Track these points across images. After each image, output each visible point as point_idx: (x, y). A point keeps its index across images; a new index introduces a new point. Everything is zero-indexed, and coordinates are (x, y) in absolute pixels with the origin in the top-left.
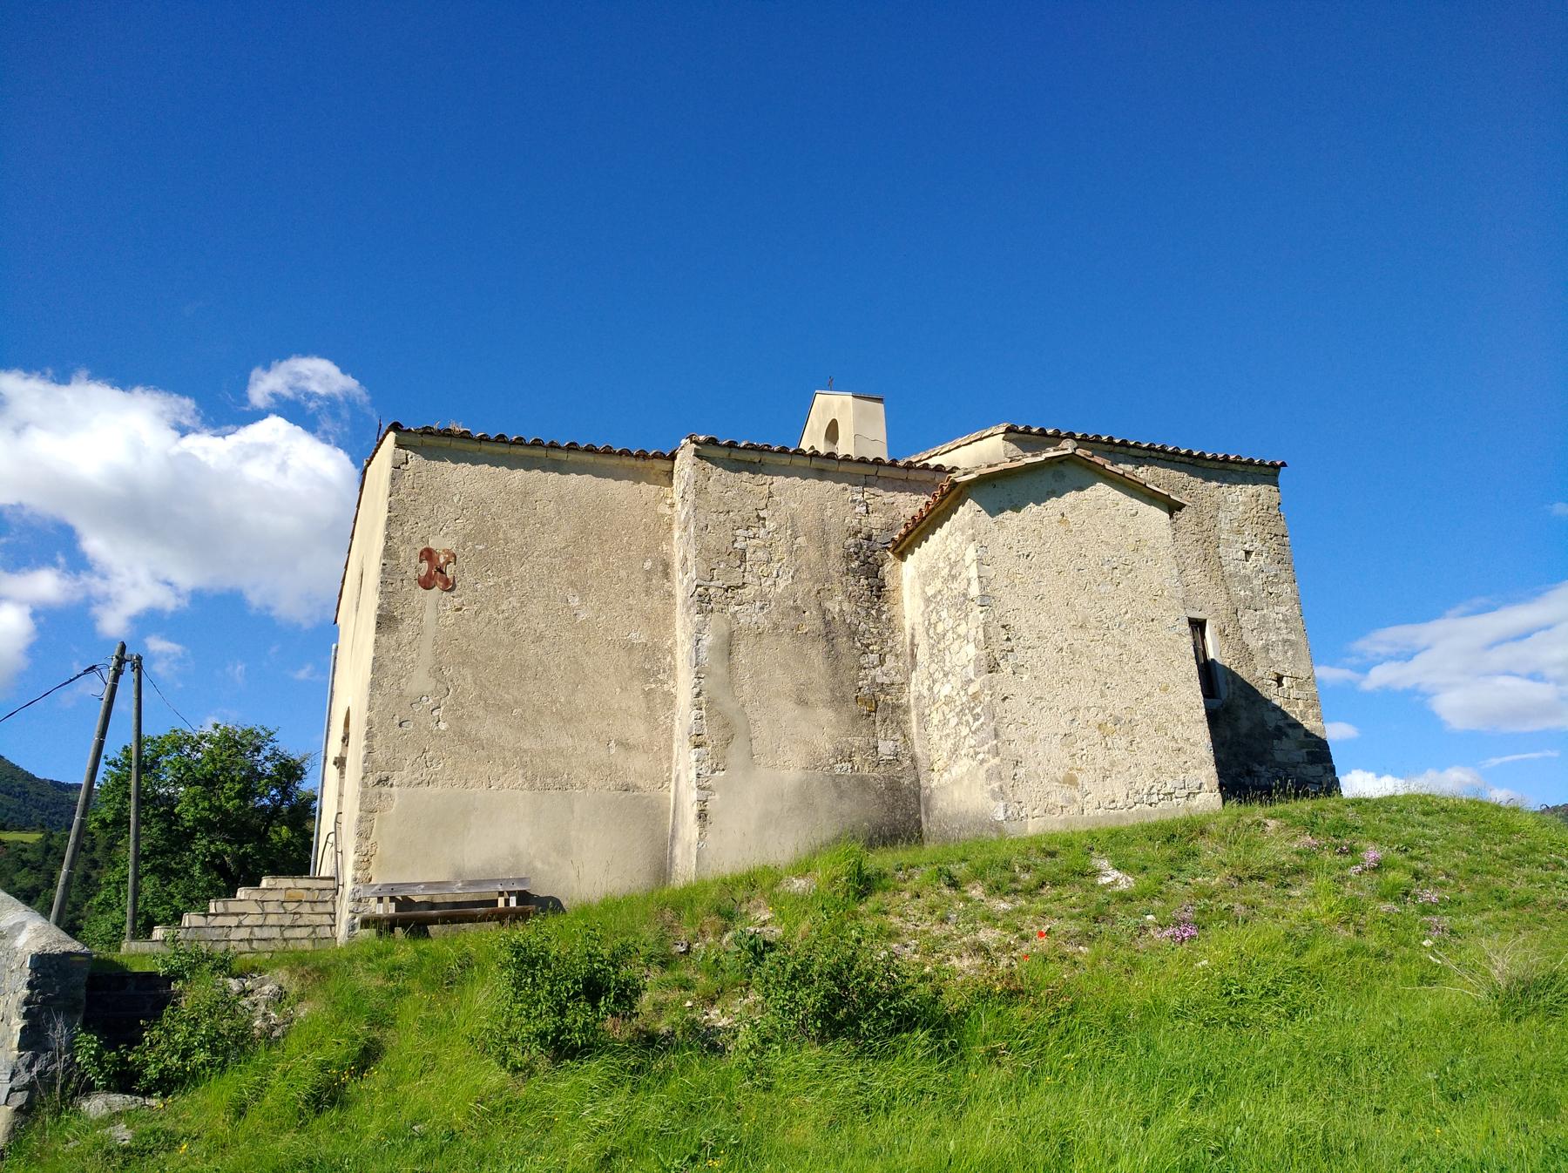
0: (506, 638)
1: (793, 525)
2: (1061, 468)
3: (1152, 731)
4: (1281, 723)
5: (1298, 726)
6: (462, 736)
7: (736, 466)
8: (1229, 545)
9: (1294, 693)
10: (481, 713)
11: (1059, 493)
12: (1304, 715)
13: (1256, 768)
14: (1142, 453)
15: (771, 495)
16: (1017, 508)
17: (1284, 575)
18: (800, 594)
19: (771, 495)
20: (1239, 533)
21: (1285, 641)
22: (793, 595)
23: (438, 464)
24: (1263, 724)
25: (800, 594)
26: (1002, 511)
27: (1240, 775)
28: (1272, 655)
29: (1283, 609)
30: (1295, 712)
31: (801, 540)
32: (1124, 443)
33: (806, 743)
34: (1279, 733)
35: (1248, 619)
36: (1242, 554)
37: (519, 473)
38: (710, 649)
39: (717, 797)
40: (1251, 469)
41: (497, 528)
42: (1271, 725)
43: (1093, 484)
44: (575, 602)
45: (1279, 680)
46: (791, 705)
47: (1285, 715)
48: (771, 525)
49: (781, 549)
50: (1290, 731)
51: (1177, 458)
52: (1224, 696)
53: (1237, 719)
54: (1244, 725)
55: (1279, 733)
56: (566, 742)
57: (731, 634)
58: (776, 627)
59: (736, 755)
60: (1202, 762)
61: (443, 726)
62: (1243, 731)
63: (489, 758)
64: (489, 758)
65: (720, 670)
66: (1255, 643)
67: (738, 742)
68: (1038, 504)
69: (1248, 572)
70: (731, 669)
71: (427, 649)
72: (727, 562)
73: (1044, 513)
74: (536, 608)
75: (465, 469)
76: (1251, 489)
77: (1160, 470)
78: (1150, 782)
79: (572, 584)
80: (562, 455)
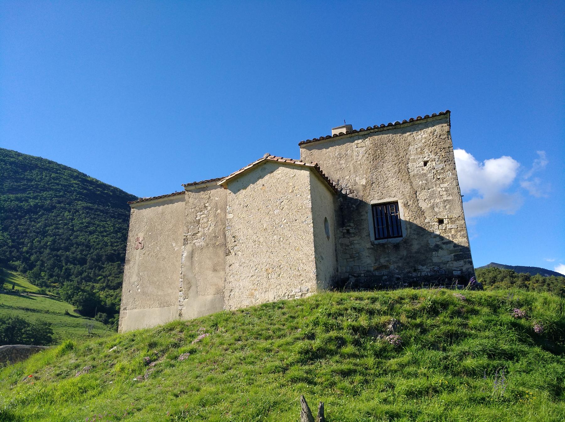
0: (155, 260)
1: (217, 206)
2: (265, 166)
3: (289, 269)
4: (439, 243)
5: (450, 242)
6: (144, 293)
7: (198, 191)
8: (414, 160)
9: (449, 226)
10: (148, 285)
11: (261, 177)
12: (454, 236)
13: (420, 267)
14: (366, 133)
15: (210, 197)
16: (245, 188)
17: (448, 167)
18: (217, 231)
19: (210, 197)
20: (421, 153)
21: (445, 201)
22: (215, 232)
23: (141, 211)
24: (427, 244)
25: (217, 231)
26: (239, 190)
27: (409, 272)
28: (436, 210)
29: (446, 185)
30: (448, 236)
31: (219, 211)
32: (390, 125)
33: (216, 285)
34: (437, 248)
35: (422, 195)
36: (422, 163)
37: (162, 207)
38: (186, 257)
39: (185, 308)
40: (429, 120)
41: (155, 226)
42: (432, 245)
43: (278, 168)
44: (174, 245)
45: (441, 222)
46: (211, 272)
47: (442, 238)
48: (209, 208)
49: (212, 215)
50: (444, 246)
51: (385, 128)
52: (404, 235)
53: (411, 245)
54: (415, 246)
55: (437, 248)
56: (170, 291)
57: (193, 251)
58: (207, 245)
59: (191, 294)
60: (310, 279)
61: (139, 290)
62: (414, 251)
63: (150, 299)
64: (150, 299)
65: (188, 264)
66: (424, 205)
67: (193, 288)
68: (253, 183)
69: (425, 172)
70: (192, 263)
71: (136, 267)
72: (193, 225)
73: (256, 187)
74: (163, 250)
75: (148, 210)
76: (430, 129)
77: (376, 137)
78: (285, 291)
79: (174, 239)
80: (172, 198)
